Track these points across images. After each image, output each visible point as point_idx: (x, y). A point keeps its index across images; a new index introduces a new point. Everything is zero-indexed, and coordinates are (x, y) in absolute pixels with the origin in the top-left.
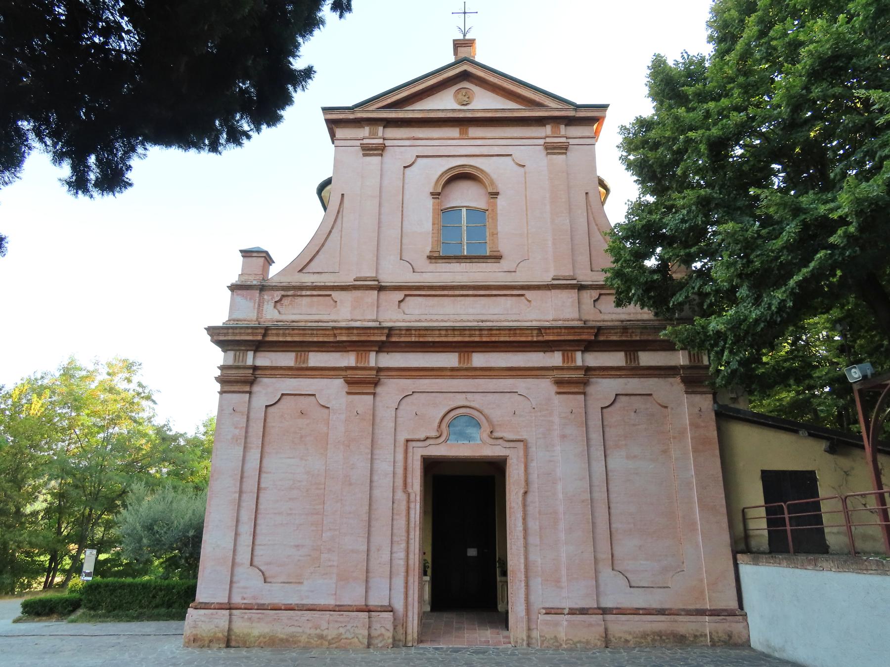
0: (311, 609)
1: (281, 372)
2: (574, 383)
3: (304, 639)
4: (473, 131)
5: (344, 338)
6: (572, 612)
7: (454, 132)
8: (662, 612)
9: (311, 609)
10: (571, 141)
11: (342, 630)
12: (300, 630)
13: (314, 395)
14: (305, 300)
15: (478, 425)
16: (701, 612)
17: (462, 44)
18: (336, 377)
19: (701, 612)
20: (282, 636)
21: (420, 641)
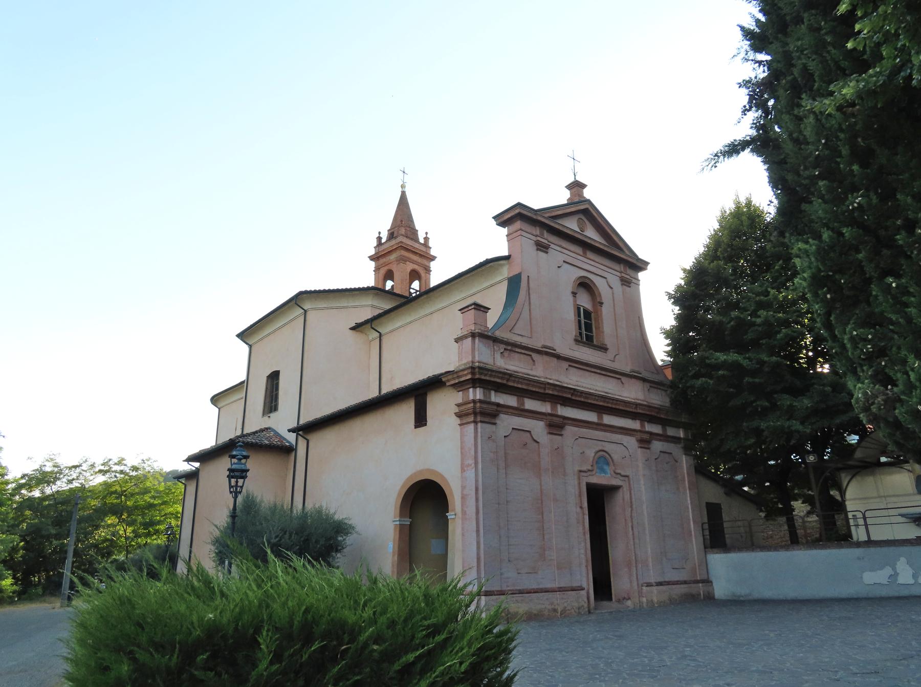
0: (546, 591)
1: (511, 411)
2: (645, 442)
3: (546, 613)
4: (590, 254)
5: (551, 392)
6: (660, 584)
7: (579, 250)
8: (685, 582)
9: (546, 591)
10: (552, 246)
11: (566, 604)
12: (543, 606)
13: (529, 432)
14: (517, 355)
15: (608, 464)
16: (697, 582)
17: (576, 187)
18: (541, 420)
19: (697, 582)
20: (535, 612)
21: (595, 609)
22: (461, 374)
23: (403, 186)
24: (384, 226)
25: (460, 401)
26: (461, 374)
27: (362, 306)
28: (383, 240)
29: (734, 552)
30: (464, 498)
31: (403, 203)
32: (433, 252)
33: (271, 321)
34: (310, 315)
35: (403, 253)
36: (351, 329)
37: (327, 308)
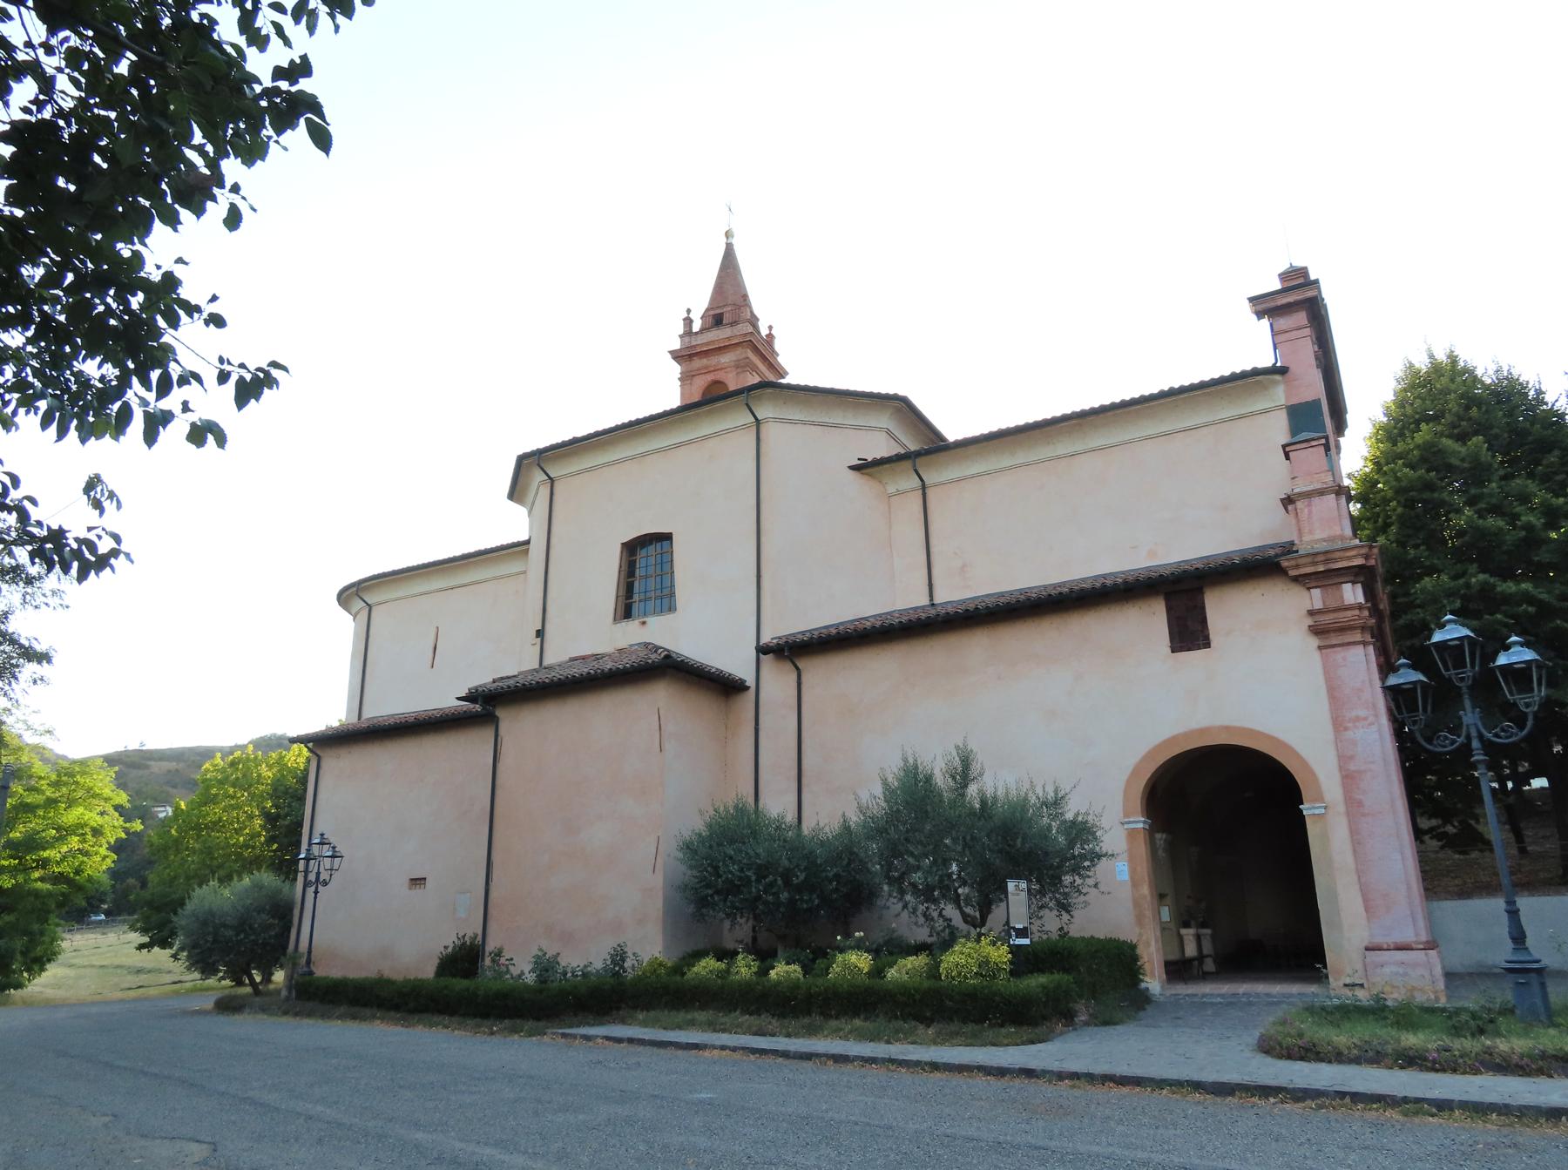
22: (1337, 555)
23: (728, 234)
24: (700, 303)
25: (1318, 605)
26: (1337, 555)
27: (871, 429)
28: (696, 327)
29: (1480, 896)
30: (1349, 779)
31: (729, 265)
32: (676, 369)
33: (644, 433)
34: (771, 432)
35: (750, 354)
36: (852, 468)
37: (804, 423)
